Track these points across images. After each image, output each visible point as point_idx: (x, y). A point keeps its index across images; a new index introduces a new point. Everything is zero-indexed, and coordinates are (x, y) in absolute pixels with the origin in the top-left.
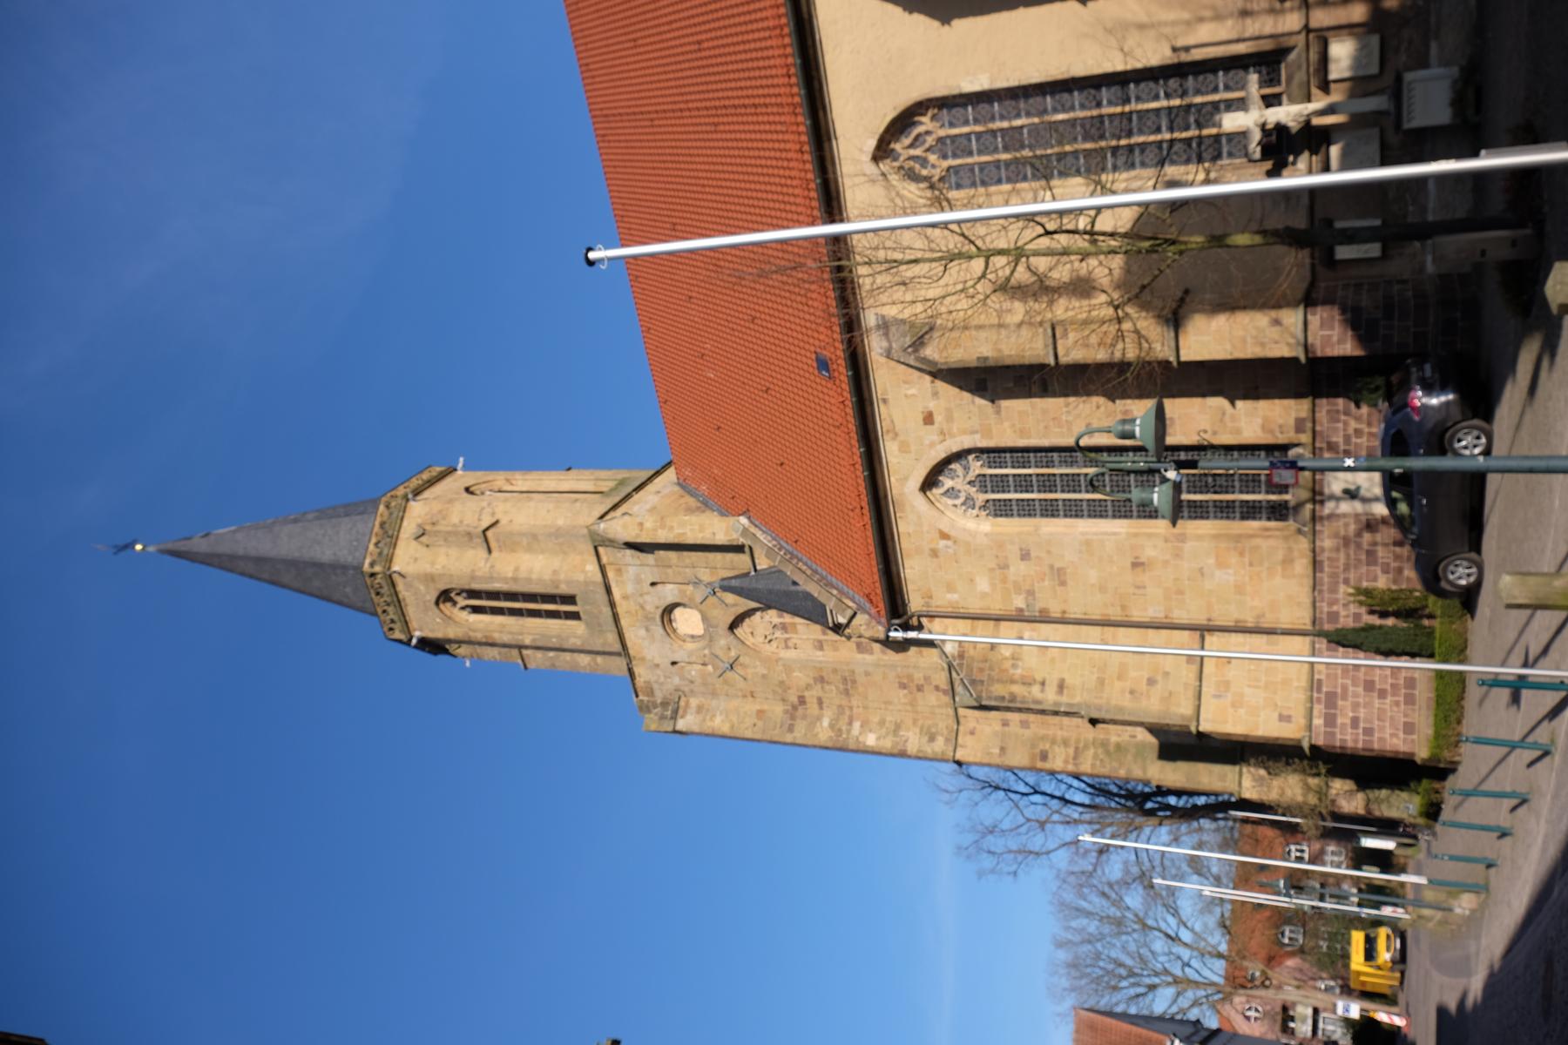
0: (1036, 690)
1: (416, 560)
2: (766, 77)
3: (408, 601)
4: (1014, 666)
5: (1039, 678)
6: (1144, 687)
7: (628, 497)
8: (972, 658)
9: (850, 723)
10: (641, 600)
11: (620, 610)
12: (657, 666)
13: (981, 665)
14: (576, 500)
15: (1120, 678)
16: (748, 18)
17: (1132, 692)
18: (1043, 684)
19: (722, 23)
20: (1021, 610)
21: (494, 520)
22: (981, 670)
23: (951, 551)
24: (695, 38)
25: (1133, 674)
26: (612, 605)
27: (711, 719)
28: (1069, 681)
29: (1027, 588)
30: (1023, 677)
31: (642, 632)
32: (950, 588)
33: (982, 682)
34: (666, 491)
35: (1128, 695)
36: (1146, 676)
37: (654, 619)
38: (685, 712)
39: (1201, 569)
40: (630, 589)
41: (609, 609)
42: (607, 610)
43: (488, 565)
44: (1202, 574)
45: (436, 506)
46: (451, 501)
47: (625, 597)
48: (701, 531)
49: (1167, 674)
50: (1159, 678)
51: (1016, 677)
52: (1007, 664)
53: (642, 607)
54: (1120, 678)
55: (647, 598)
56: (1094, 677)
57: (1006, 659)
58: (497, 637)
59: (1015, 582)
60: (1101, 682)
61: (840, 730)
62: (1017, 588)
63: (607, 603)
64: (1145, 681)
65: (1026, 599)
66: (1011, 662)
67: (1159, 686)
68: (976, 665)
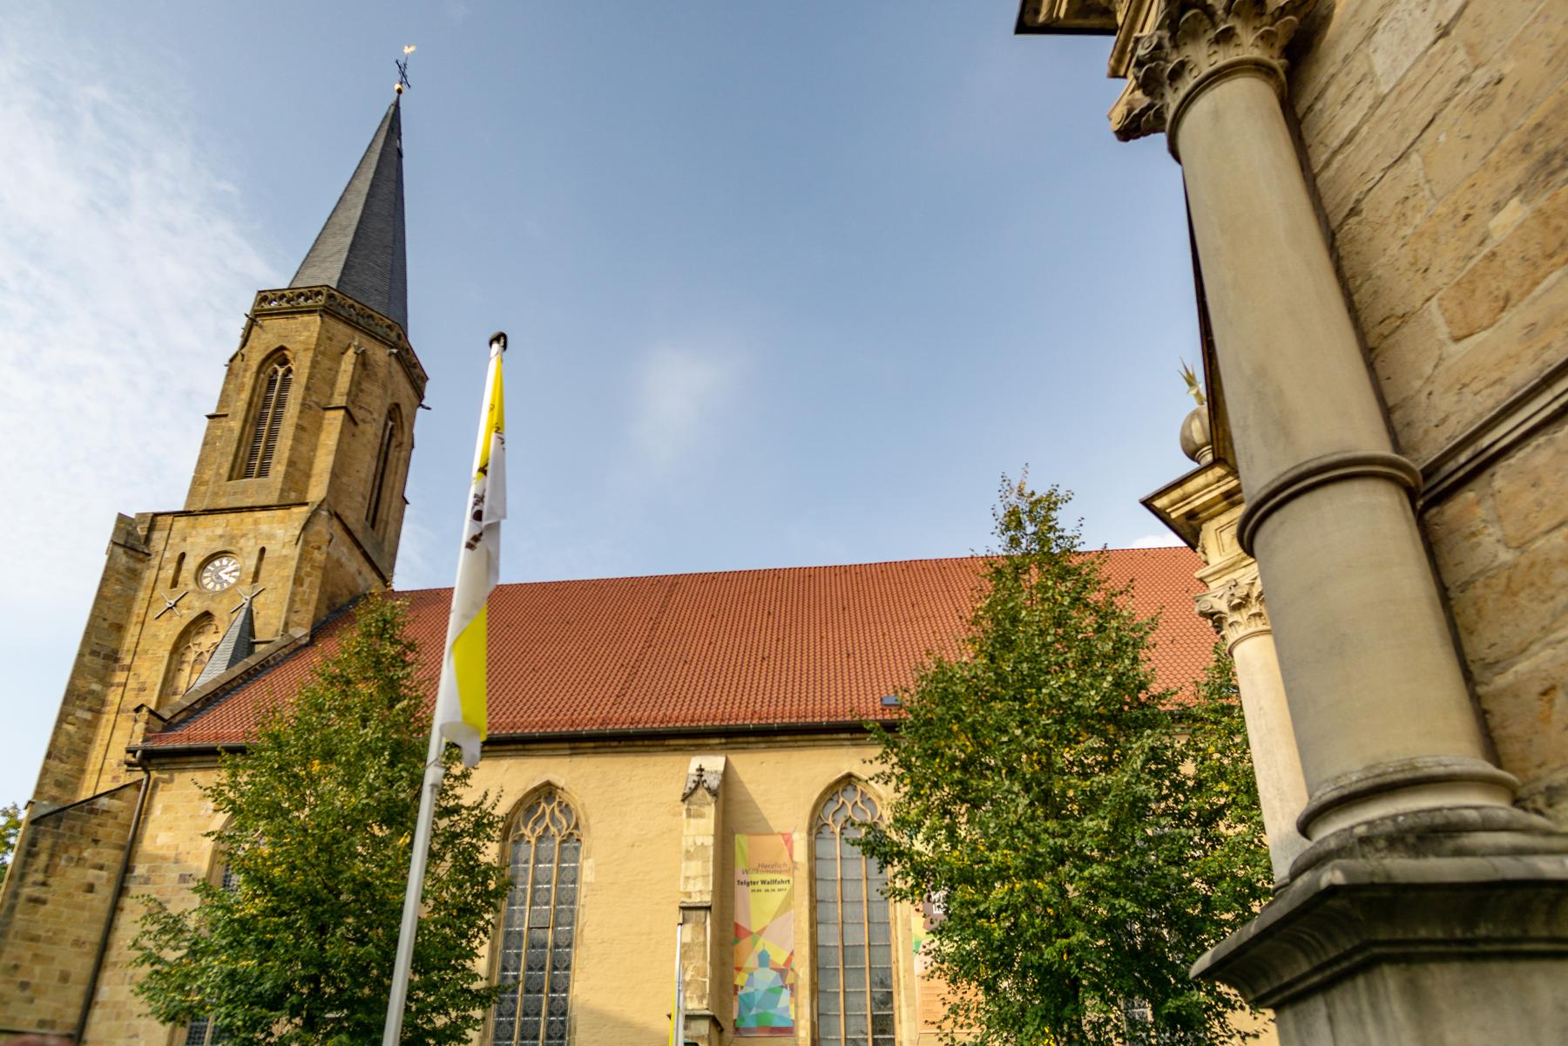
0: (40, 877)
1: (330, 339)
2: (720, 673)
3: (291, 321)
4: (70, 859)
5: (51, 881)
6: (20, 979)
7: (358, 545)
8: (88, 821)
9: (90, 710)
10: (251, 536)
11: (245, 515)
12: (184, 540)
13: (77, 830)
14: (364, 498)
15: (36, 956)
16: (873, 596)
17: (16, 967)
18: (44, 884)
19: (806, 620)
20: (132, 871)
21: (357, 420)
22: (71, 829)
23: (202, 812)
24: (766, 615)
25: (38, 969)
26: (251, 509)
27: (117, 580)
28: (43, 909)
29: (153, 878)
30: (56, 866)
31: (219, 531)
32: (166, 809)
33: (58, 827)
34: (360, 580)
35: (13, 963)
36: (32, 981)
37: (231, 544)
38: (131, 557)
39: (136, 1036)
40: (264, 528)
41: (249, 505)
42: (248, 502)
43: (312, 404)
44: (131, 1037)
45: (382, 373)
46: (384, 387)
47: (256, 522)
48: (301, 600)
49: (31, 1001)
50: (27, 993)
51: (57, 860)
52: (74, 853)
53: (243, 536)
54: (36, 956)
55: (252, 542)
56: (41, 932)
57: (81, 852)
58: (800, 1010)
59: (160, 867)
60: (35, 939)
61: (85, 699)
62: (152, 870)
63: (256, 504)
64: (26, 979)
65: (142, 876)
66: (76, 856)
67: (18, 993)
68: (79, 823)
